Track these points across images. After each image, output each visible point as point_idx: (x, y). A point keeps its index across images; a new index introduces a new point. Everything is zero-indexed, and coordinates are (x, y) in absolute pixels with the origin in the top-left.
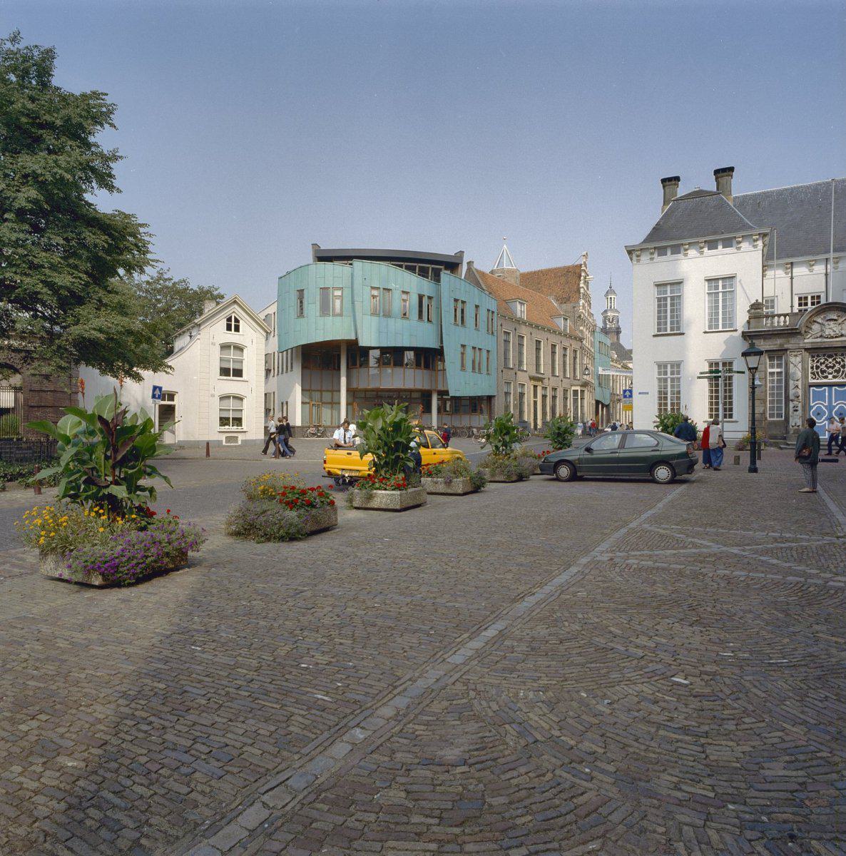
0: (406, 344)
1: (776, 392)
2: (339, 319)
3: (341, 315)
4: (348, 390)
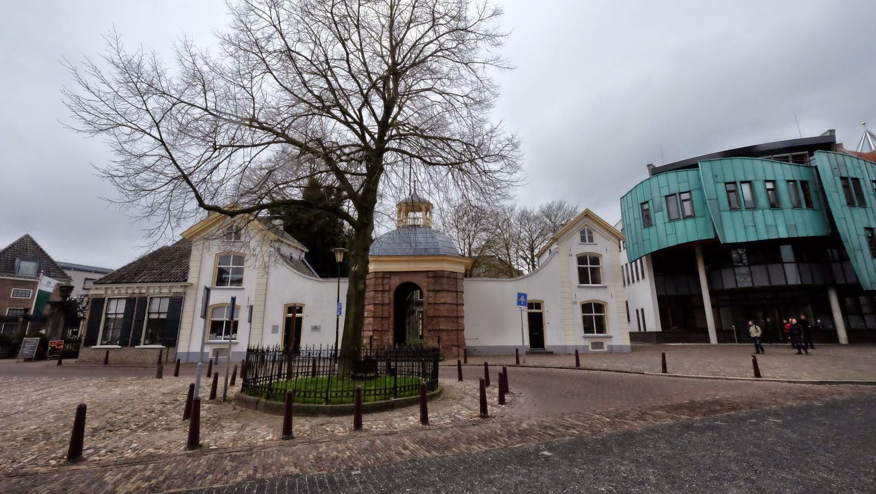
0: (783, 234)
1: (263, 400)
2: (690, 222)
3: (692, 216)
4: (712, 294)
